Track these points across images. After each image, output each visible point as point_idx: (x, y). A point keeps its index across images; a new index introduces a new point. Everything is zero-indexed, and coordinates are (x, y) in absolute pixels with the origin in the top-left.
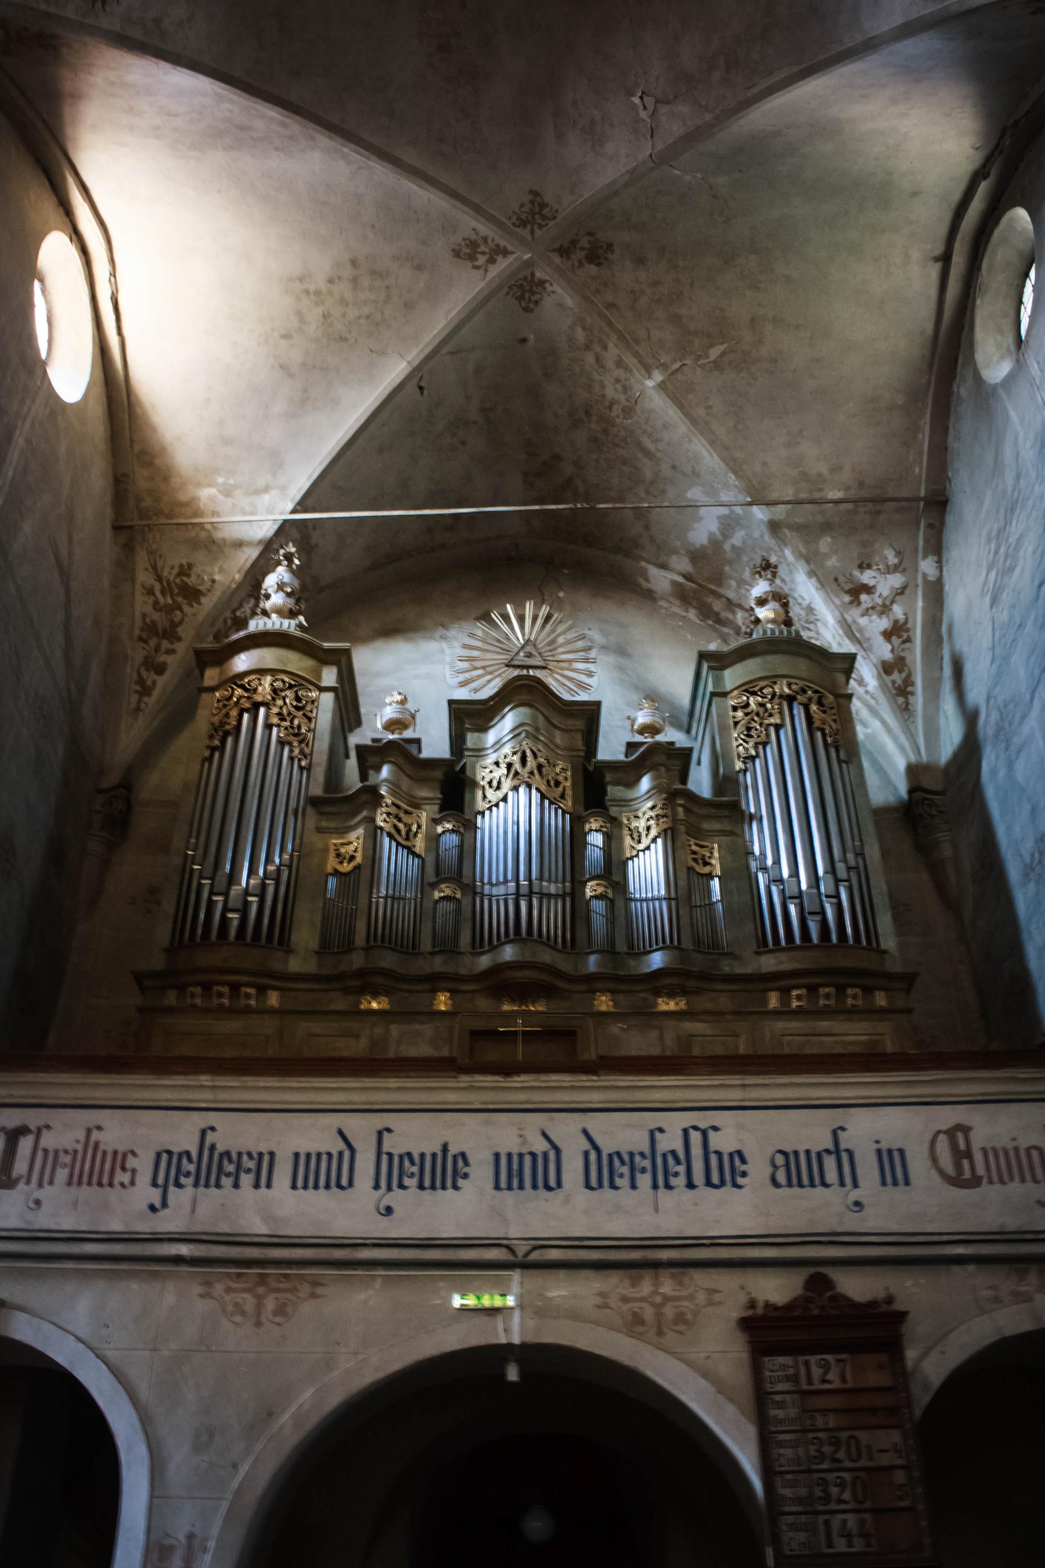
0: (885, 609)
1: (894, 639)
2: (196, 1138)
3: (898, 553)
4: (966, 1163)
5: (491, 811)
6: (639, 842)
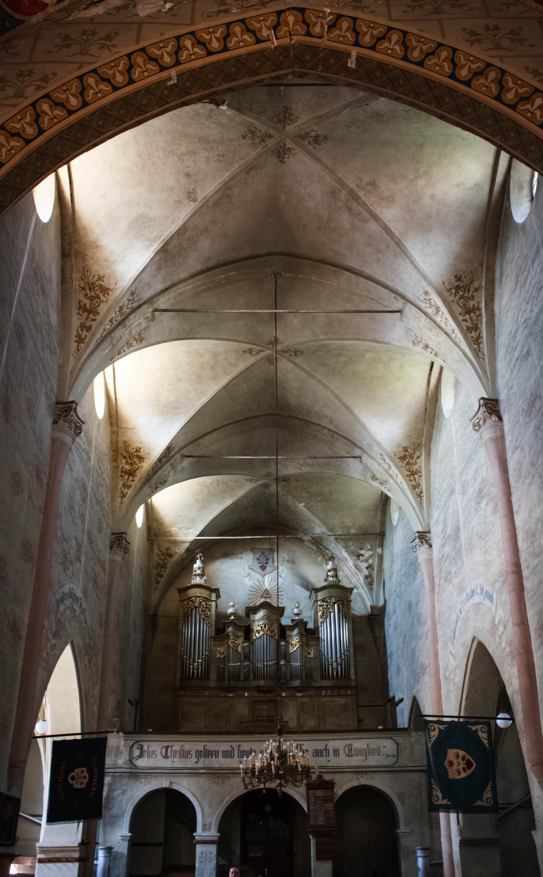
0: (367, 561)
2: (203, 748)
3: (371, 546)
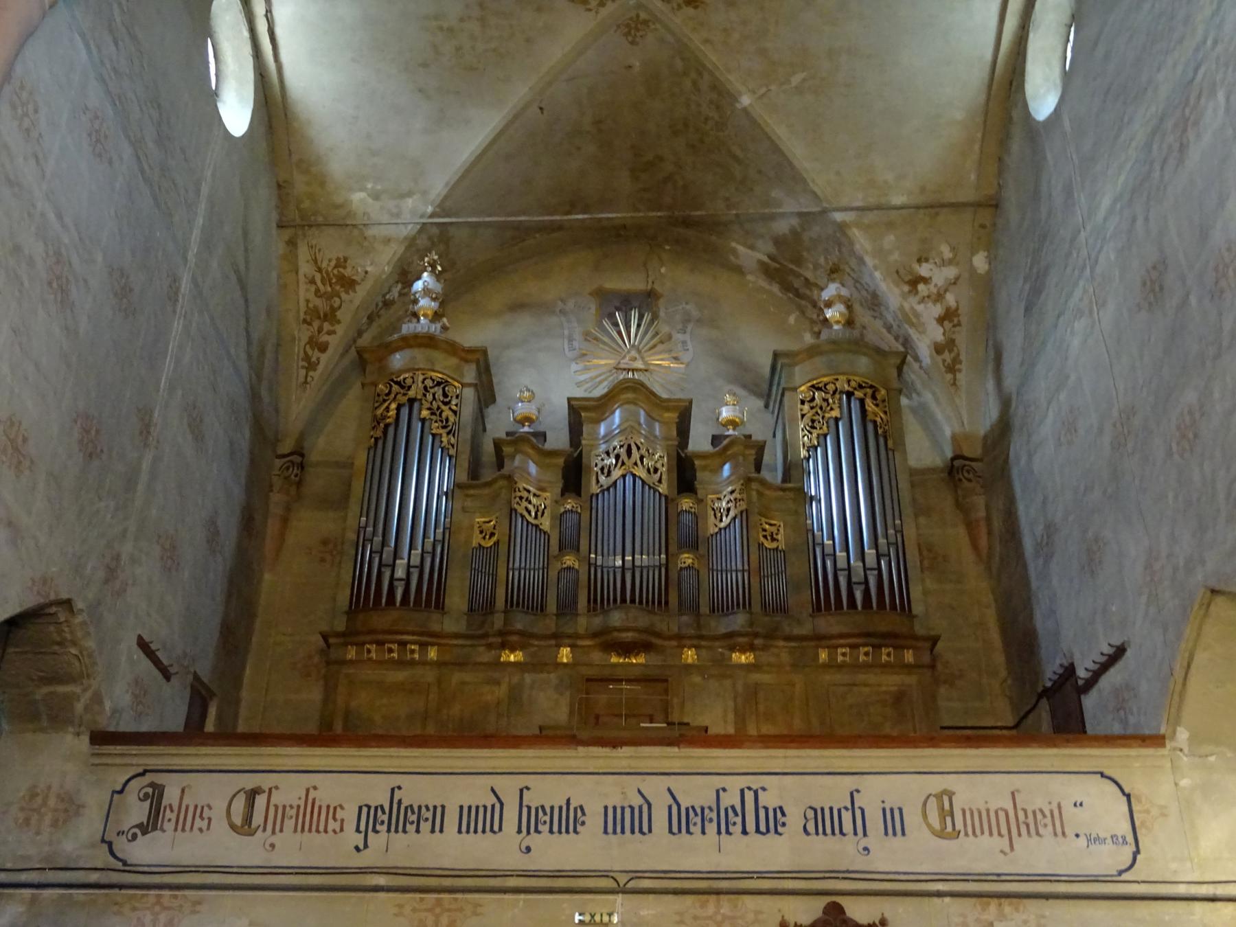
0: (939, 297)
1: (946, 323)
3: (953, 249)
4: (949, 820)
5: (603, 494)
6: (721, 520)
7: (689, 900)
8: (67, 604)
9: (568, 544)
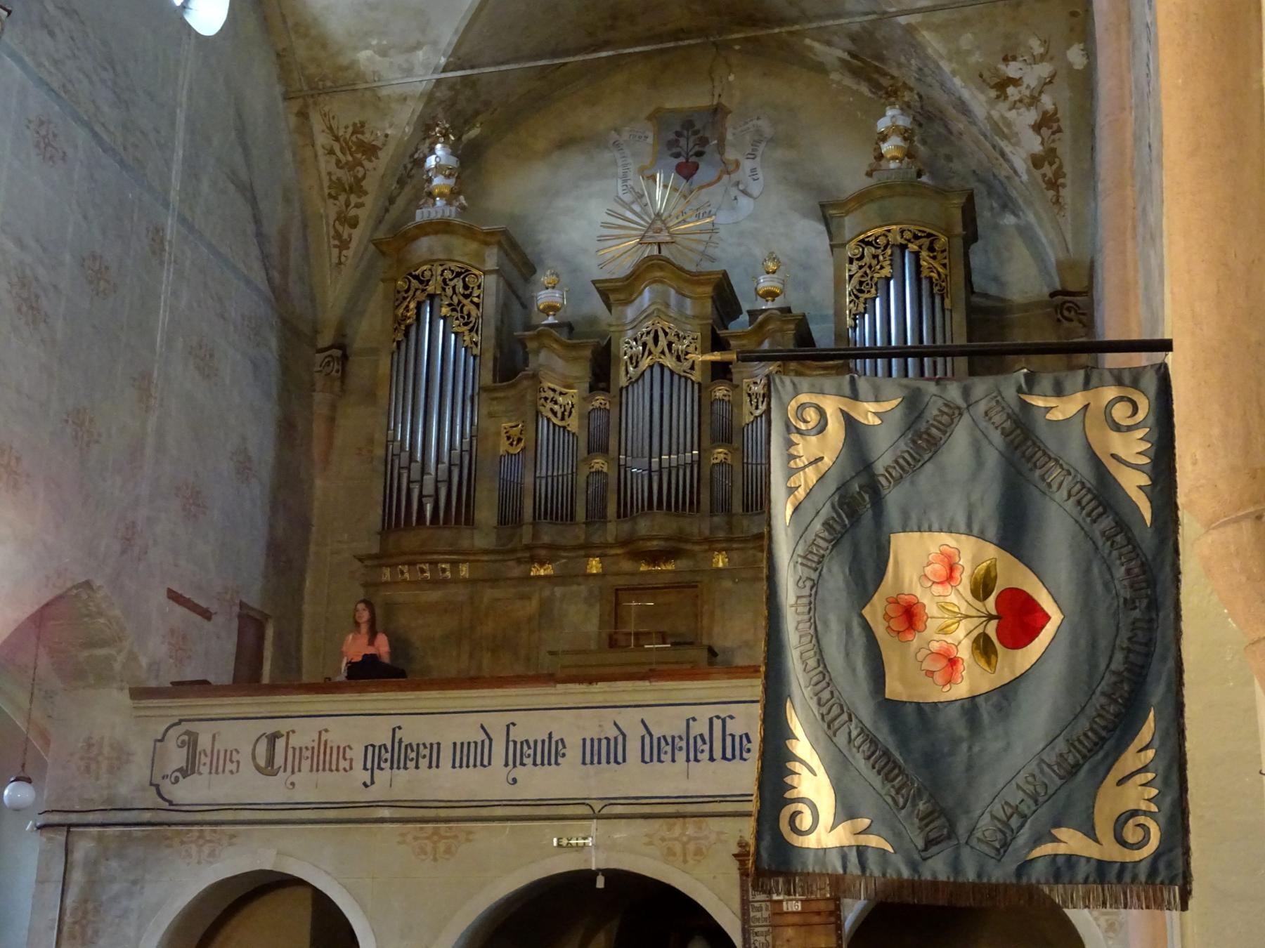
0: (1034, 100)
1: (1044, 131)
3: (1044, 42)
6: (757, 408)
7: (657, 823)
8: (87, 584)
9: (598, 446)
